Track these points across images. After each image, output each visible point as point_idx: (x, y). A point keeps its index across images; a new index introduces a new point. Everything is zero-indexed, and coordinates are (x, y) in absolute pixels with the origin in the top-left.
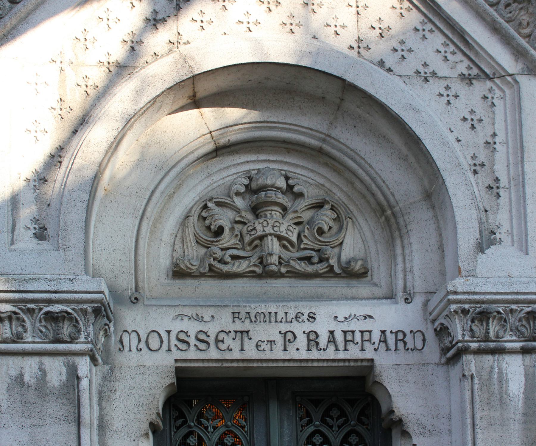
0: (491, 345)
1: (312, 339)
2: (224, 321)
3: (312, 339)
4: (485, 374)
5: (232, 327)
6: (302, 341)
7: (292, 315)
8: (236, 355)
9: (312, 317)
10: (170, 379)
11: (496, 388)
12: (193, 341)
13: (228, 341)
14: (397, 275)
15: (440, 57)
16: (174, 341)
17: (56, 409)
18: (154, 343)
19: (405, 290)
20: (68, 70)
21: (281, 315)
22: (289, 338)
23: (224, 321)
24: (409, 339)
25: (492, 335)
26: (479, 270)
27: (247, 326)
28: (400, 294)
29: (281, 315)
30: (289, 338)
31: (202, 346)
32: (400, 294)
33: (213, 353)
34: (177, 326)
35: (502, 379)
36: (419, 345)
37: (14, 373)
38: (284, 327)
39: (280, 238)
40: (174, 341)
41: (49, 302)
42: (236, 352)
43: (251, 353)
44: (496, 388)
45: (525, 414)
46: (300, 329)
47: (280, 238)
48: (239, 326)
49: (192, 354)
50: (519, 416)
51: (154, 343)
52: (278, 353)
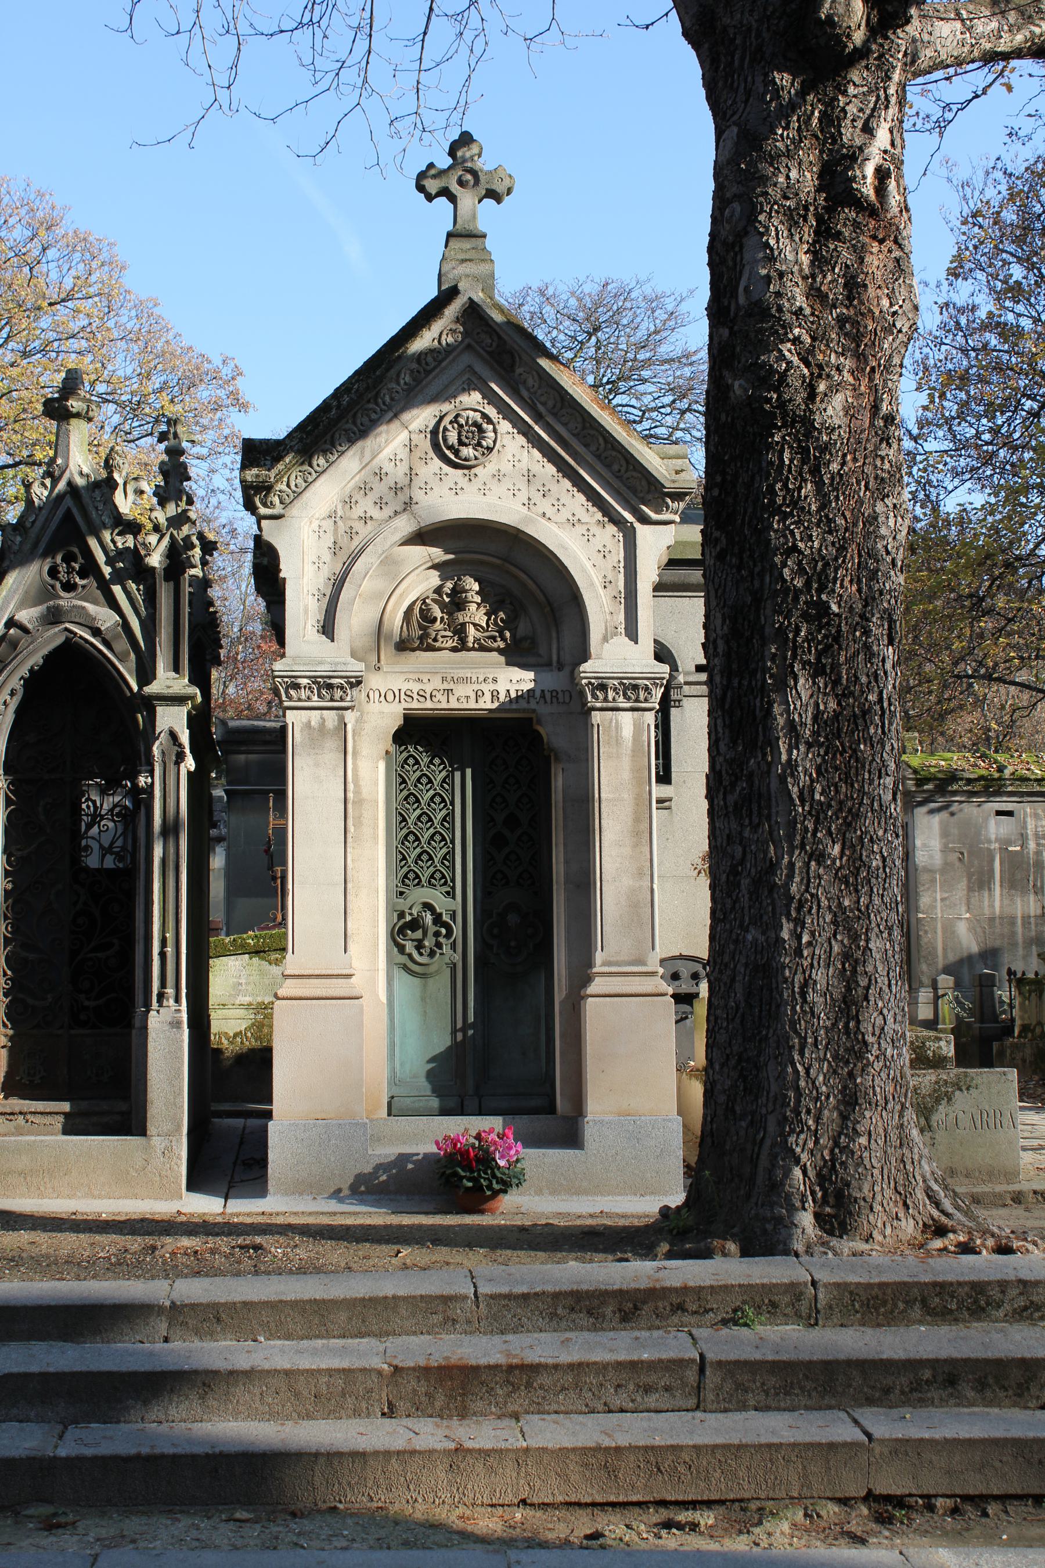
0: (610, 705)
1: (495, 695)
2: (436, 683)
3: (495, 695)
4: (606, 723)
5: (442, 687)
6: (488, 696)
7: (481, 679)
8: (444, 705)
9: (495, 680)
10: (746, 1259)
11: (614, 734)
12: (415, 696)
13: (439, 696)
14: (274, 1278)
15: (584, 509)
16: (403, 696)
17: (332, 744)
18: (390, 697)
19: (558, 662)
20: (340, 523)
21: (474, 679)
22: (478, 695)
23: (436, 683)
24: (560, 695)
25: (610, 698)
26: (605, 654)
27: (451, 686)
28: (555, 663)
29: (474, 679)
30: (478, 695)
31: (422, 699)
32: (555, 663)
33: (429, 704)
34: (405, 687)
35: (618, 727)
36: (567, 700)
37: (304, 720)
38: (476, 687)
39: (475, 625)
40: (403, 696)
41: (330, 677)
42: (442, 704)
43: (454, 704)
44: (614, 734)
45: (633, 751)
46: (487, 688)
47: (475, 625)
48: (446, 686)
49: (415, 705)
50: (629, 752)
51: (390, 697)
52: (472, 705)
